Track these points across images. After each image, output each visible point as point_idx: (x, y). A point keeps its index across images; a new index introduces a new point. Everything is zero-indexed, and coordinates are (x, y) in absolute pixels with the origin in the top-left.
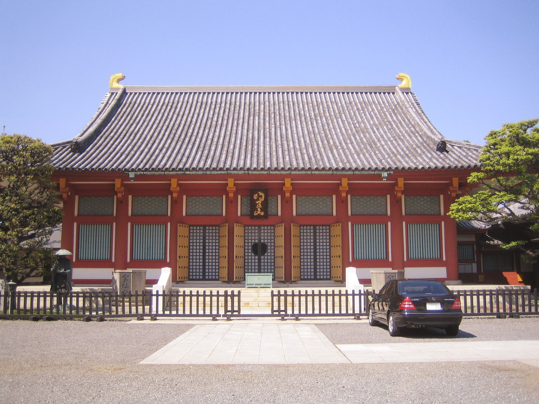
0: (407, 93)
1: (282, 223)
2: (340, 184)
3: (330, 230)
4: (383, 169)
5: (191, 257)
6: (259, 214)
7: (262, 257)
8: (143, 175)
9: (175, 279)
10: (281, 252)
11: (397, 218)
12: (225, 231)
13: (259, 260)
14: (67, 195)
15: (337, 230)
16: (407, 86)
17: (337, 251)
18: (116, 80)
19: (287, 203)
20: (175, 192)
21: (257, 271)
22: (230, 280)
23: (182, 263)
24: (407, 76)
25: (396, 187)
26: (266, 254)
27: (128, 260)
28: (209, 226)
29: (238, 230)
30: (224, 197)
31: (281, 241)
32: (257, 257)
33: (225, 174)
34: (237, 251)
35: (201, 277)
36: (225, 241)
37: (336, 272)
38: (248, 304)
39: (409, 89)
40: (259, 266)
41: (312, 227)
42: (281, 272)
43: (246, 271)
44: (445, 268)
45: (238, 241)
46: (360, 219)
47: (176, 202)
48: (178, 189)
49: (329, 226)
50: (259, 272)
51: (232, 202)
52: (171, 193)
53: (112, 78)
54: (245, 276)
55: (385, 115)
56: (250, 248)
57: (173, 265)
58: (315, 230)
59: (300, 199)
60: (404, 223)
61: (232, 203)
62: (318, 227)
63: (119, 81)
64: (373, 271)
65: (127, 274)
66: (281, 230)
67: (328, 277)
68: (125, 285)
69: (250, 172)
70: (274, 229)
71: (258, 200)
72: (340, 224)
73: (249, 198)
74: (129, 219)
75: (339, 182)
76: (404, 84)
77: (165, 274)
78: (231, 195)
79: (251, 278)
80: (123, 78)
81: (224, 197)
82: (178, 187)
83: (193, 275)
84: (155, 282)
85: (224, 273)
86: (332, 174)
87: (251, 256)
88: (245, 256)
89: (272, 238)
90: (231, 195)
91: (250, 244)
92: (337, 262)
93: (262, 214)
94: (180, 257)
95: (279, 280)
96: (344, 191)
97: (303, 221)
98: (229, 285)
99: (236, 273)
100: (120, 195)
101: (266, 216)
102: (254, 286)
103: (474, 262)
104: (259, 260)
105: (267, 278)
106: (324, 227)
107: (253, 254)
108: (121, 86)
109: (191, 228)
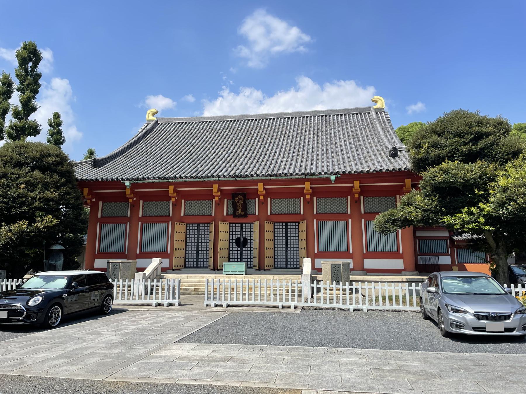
0: (381, 113)
1: (304, 220)
4: (332, 173)
6: (240, 214)
7: (244, 249)
10: (256, 244)
11: (357, 216)
12: (303, 226)
13: (241, 251)
14: (133, 200)
16: (381, 107)
17: (303, 244)
18: (151, 114)
19: (263, 203)
21: (239, 260)
22: (216, 269)
29: (223, 227)
31: (256, 236)
32: (239, 249)
35: (195, 266)
39: (383, 109)
40: (241, 256)
41: (284, 224)
44: (96, 260)
45: (223, 236)
46: (322, 216)
48: (264, 192)
51: (263, 203)
52: (258, 196)
55: (356, 131)
56: (234, 241)
58: (198, 227)
59: (187, 202)
60: (363, 220)
62: (244, 225)
63: (153, 114)
65: (117, 264)
68: (115, 273)
69: (220, 179)
71: (238, 202)
74: (98, 220)
76: (378, 106)
78: (308, 197)
79: (228, 267)
83: (277, 264)
86: (288, 178)
87: (235, 248)
91: (234, 238)
92: (303, 252)
93: (243, 213)
100: (217, 198)
101: (246, 215)
102: (230, 273)
103: (449, 255)
104: (241, 251)
105: (242, 267)
106: (281, 224)
108: (155, 119)
109: (276, 224)
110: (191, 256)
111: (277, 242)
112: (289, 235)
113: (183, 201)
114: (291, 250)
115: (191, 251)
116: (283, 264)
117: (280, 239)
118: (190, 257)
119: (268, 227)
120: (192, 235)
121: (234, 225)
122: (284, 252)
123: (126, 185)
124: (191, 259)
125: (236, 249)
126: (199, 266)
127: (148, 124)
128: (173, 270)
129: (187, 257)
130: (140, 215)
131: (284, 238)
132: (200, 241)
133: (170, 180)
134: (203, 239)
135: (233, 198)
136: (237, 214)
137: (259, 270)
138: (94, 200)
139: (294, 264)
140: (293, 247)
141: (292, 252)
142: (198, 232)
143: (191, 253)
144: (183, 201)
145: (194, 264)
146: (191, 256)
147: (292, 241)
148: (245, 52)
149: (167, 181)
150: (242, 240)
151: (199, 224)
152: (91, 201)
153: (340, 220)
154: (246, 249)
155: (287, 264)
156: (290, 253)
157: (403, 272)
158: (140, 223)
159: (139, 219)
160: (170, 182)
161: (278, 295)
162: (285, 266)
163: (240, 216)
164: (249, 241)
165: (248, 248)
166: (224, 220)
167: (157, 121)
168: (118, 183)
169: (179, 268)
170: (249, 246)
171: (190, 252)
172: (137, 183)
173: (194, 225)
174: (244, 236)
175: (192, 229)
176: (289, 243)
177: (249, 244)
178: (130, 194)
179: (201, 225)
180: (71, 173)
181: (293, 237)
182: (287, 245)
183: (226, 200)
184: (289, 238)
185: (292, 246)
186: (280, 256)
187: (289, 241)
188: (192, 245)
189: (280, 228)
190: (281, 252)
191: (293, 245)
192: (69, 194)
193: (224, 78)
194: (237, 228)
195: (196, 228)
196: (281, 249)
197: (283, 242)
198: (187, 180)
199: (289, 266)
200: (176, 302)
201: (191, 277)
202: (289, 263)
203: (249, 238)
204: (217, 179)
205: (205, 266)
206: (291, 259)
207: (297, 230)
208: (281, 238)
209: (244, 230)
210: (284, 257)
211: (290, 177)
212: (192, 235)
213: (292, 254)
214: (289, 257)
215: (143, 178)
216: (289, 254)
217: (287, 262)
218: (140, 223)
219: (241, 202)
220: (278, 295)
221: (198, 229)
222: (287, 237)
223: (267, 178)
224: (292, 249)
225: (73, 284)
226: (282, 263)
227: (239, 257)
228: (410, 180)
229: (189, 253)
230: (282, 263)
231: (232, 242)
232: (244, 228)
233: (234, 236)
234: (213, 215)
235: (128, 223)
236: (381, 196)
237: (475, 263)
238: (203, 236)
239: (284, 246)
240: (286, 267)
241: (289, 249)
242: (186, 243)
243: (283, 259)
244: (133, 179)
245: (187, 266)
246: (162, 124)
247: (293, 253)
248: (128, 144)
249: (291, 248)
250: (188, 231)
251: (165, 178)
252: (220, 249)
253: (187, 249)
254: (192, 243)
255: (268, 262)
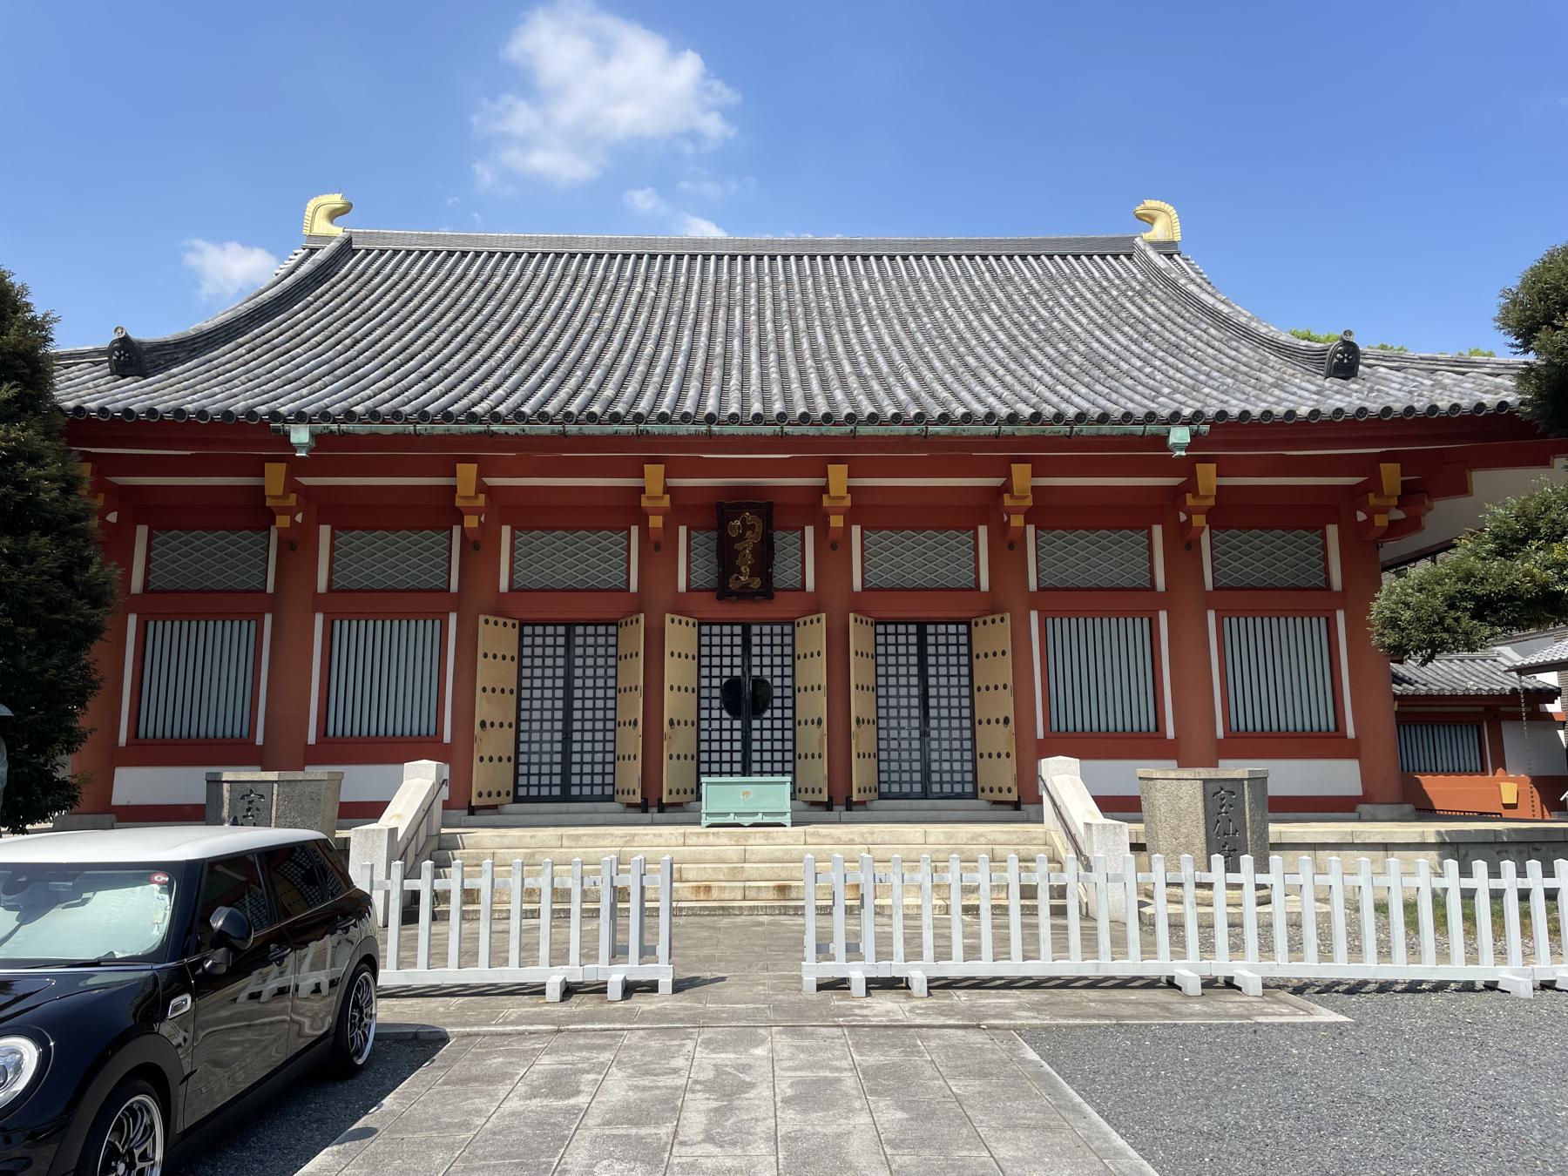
2: (1007, 488)
3: (969, 634)
4: (1175, 418)
5: (968, 755)
6: (746, 586)
7: (756, 724)
8: (340, 445)
9: (462, 803)
10: (815, 705)
12: (634, 637)
15: (994, 636)
18: (322, 213)
19: (833, 548)
20: (475, 511)
21: (737, 767)
22: (655, 803)
23: (493, 743)
24: (1162, 205)
25: (1189, 496)
26: (768, 714)
27: (123, 739)
28: (585, 624)
29: (679, 636)
30: (635, 530)
31: (814, 671)
33: (633, 444)
34: (675, 704)
35: (556, 791)
36: (634, 673)
37: (1001, 774)
38: (708, 889)
40: (746, 751)
41: (913, 629)
42: (817, 773)
43: (704, 767)
45: (677, 672)
47: (476, 547)
49: (969, 624)
50: (746, 772)
51: (657, 547)
53: (311, 205)
54: (699, 784)
56: (716, 693)
57: (453, 754)
58: (569, 636)
60: (1211, 615)
61: (657, 549)
63: (333, 215)
64: (1159, 769)
65: (261, 789)
66: (813, 636)
67: (969, 788)
69: (715, 428)
70: (793, 634)
71: (741, 538)
72: (1007, 616)
73: (714, 534)
75: (996, 482)
76: (1159, 232)
77: (417, 782)
79: (720, 794)
80: (345, 210)
81: (635, 530)
82: (482, 497)
84: (374, 810)
85: (631, 775)
86: (997, 436)
88: (699, 719)
89: (788, 661)
90: (656, 522)
91: (716, 682)
94: (483, 724)
95: (811, 797)
96: (1016, 510)
97: (892, 609)
98: (646, 817)
99: (672, 777)
101: (767, 592)
102: (730, 819)
105: (774, 794)
106: (902, 629)
107: (725, 714)
108: (338, 232)
110: (541, 753)
111: (960, 686)
112: (932, 671)
113: (506, 531)
114: (939, 729)
115: (541, 731)
116: (911, 782)
117: (898, 686)
118: (535, 758)
119: (859, 636)
120: (543, 667)
121: (716, 629)
122: (916, 734)
123: (294, 439)
124: (540, 764)
125: (726, 724)
126: (575, 791)
127: (313, 251)
128: (472, 811)
129: (523, 758)
130: (322, 586)
131: (914, 681)
132: (578, 693)
133: (495, 428)
134: (589, 683)
135: (721, 527)
136: (733, 586)
137: (644, 807)
138: (112, 517)
139: (952, 783)
140: (950, 718)
141: (945, 734)
142: (569, 657)
143: (541, 742)
144: (506, 531)
145: (550, 785)
146: (541, 753)
147: (943, 692)
148: (522, 118)
149: (482, 428)
150: (749, 687)
151: (570, 625)
152: (106, 525)
153: (1126, 613)
154: (767, 724)
155: (566, 785)
156: (939, 739)
157: (1363, 808)
158: (319, 618)
159: (318, 603)
160: (494, 434)
161: (986, 912)
162: (917, 788)
163: (745, 594)
164: (777, 692)
165: (772, 719)
166: (680, 607)
167: (349, 241)
168: (253, 436)
169: (494, 800)
170: (778, 713)
171: (536, 737)
172: (345, 434)
173: (550, 630)
174: (756, 672)
175: (544, 646)
176: (933, 702)
177: (777, 703)
178: (286, 495)
179: (579, 630)
180: (40, 370)
181: (948, 676)
182: (925, 707)
183: (683, 530)
184: (932, 681)
185: (944, 713)
186: (899, 750)
187: (932, 692)
188: (542, 710)
189: (897, 645)
190: (904, 734)
191: (949, 708)
192: (34, 459)
193: (450, 201)
194: (727, 640)
195: (561, 641)
196: (904, 723)
197: (909, 697)
198: (572, 429)
199: (936, 788)
200: (663, 974)
201: (577, 838)
202: (935, 777)
203: (777, 682)
204: (704, 428)
205: (598, 791)
206: (941, 761)
207: (611, 683)
208: (903, 681)
209: (755, 650)
210: (916, 755)
211: (1007, 429)
212: (543, 667)
213: (945, 745)
214: (935, 755)
215: (374, 415)
216: (934, 745)
217: (926, 772)
218: (319, 618)
219: (752, 538)
220: (986, 912)
221: (569, 646)
222: (923, 676)
223: (915, 430)
224: (945, 723)
225: (218, 923)
226: (906, 777)
227: (737, 757)
228: (1397, 466)
229: (530, 742)
230: (906, 777)
231: (710, 698)
232: (755, 640)
233: (716, 672)
234: (634, 587)
235: (268, 618)
236: (1295, 528)
237: (1448, 773)
238: (590, 672)
239: (915, 713)
240: (925, 795)
241: (933, 723)
242: (519, 699)
243: (911, 761)
244: (325, 416)
245: (522, 792)
246: (368, 252)
247: (951, 740)
248: (250, 305)
249: (939, 718)
250: (527, 651)
251: (473, 418)
252: (671, 722)
253: (524, 726)
254: (542, 699)
255: (861, 774)
